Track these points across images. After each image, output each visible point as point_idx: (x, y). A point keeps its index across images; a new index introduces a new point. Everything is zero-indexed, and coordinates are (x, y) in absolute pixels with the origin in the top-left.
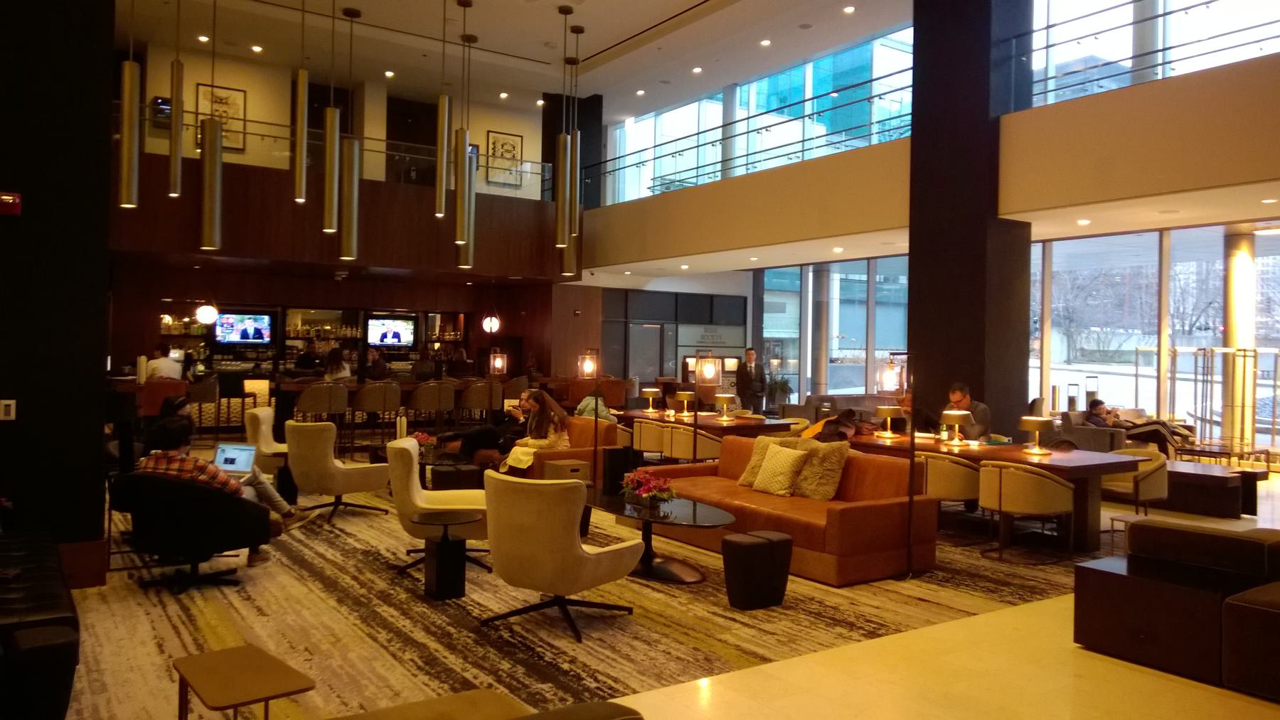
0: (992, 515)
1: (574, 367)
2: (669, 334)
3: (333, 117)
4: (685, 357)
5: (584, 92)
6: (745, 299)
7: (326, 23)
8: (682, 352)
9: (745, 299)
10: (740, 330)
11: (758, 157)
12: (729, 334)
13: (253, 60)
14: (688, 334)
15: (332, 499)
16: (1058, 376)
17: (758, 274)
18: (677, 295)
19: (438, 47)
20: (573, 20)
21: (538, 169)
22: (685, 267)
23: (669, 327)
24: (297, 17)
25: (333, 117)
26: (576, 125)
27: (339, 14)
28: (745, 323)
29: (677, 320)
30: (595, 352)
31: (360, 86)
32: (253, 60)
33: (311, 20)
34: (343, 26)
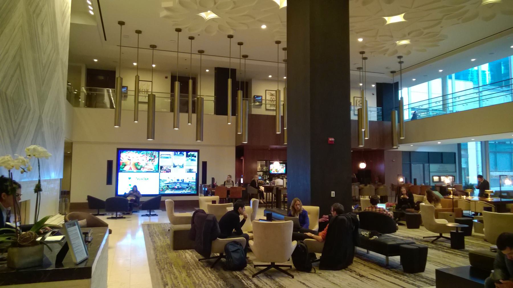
0: (457, 231)
1: (398, 181)
2: (426, 168)
3: (240, 93)
4: (433, 176)
5: (395, 81)
6: (455, 153)
7: (238, 61)
8: (431, 174)
9: (455, 153)
10: (453, 165)
11: (433, 101)
12: (450, 167)
13: (153, 70)
14: (434, 167)
15: (438, 235)
16: (194, 165)
17: (459, 145)
18: (428, 153)
19: (276, 65)
20: (364, 55)
21: (376, 109)
22: (439, 143)
23: (426, 165)
24: (175, 54)
25: (240, 93)
26: (387, 95)
27: (241, 57)
28: (455, 163)
29: (429, 162)
30: (403, 176)
31: (250, 80)
32: (153, 70)
33: (232, 60)
34: (243, 61)
